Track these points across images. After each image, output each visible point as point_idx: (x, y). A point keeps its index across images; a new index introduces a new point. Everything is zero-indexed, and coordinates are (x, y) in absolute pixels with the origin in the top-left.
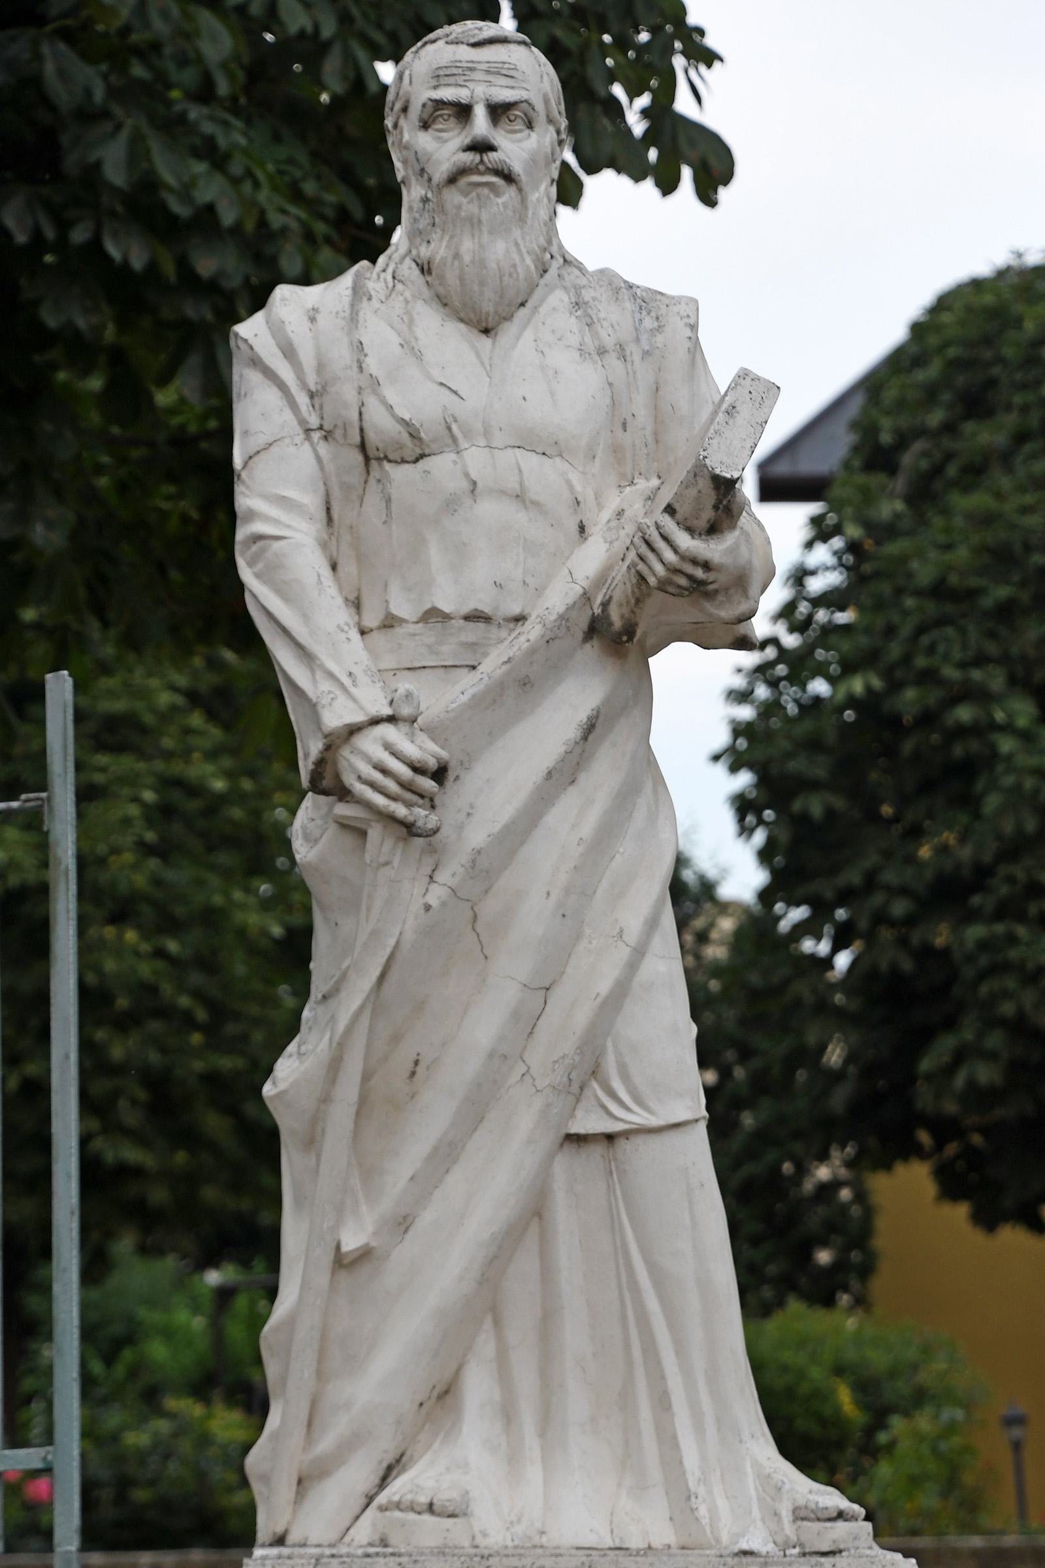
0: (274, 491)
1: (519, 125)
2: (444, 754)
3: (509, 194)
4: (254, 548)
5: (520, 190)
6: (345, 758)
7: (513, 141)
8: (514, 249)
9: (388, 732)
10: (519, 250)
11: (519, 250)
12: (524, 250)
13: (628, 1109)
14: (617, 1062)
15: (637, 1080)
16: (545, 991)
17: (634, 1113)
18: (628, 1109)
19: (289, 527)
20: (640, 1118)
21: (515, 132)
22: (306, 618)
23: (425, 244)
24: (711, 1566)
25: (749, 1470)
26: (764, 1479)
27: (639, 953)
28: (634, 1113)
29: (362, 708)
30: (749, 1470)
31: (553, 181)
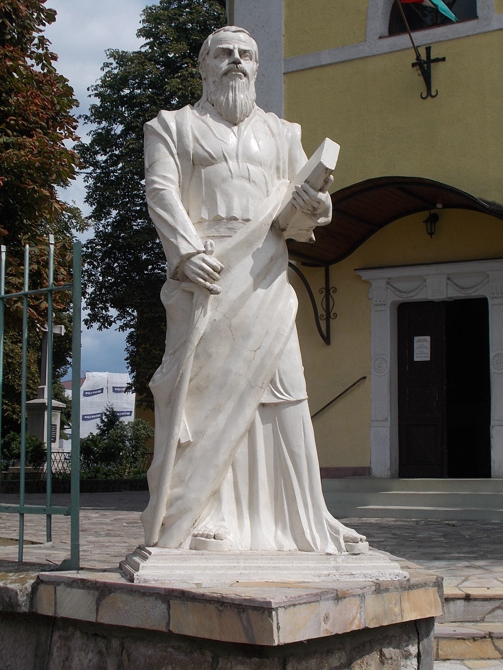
0: (161, 174)
1: (248, 58)
2: (223, 266)
3: (244, 80)
4: (153, 194)
5: (248, 79)
6: (187, 265)
7: (246, 63)
8: (246, 97)
9: (202, 255)
10: (247, 98)
11: (247, 98)
12: (249, 99)
13: (283, 395)
14: (279, 378)
15: (286, 384)
16: (254, 352)
17: (284, 395)
18: (283, 395)
19: (166, 186)
20: (287, 397)
21: (247, 60)
22: (173, 216)
23: (214, 96)
24: (17, 388)
25: (325, 523)
26: (331, 526)
27: (288, 339)
28: (284, 395)
29: (194, 248)
30: (325, 523)
31: (78, 573)
